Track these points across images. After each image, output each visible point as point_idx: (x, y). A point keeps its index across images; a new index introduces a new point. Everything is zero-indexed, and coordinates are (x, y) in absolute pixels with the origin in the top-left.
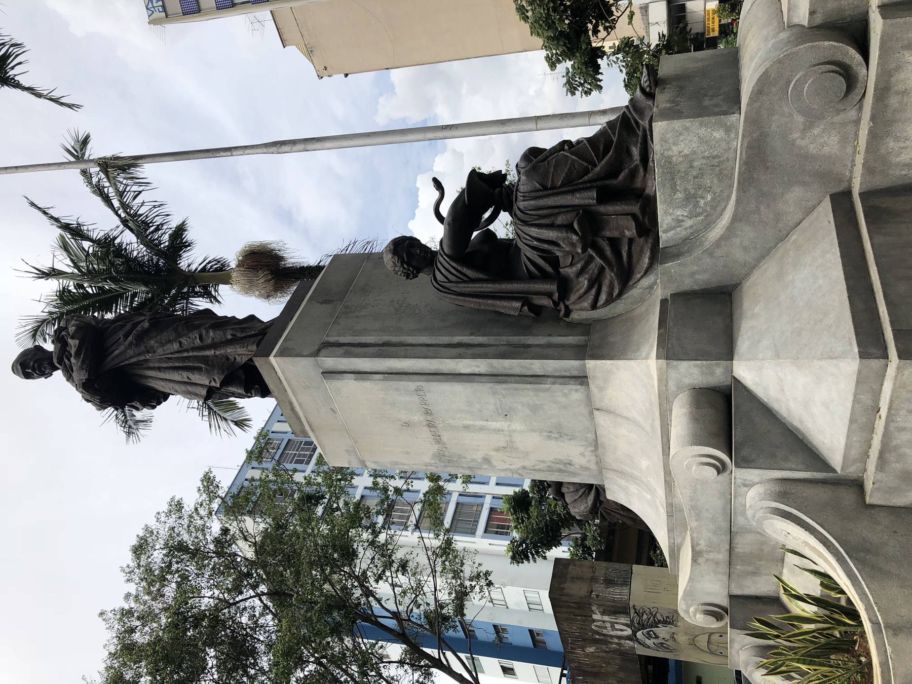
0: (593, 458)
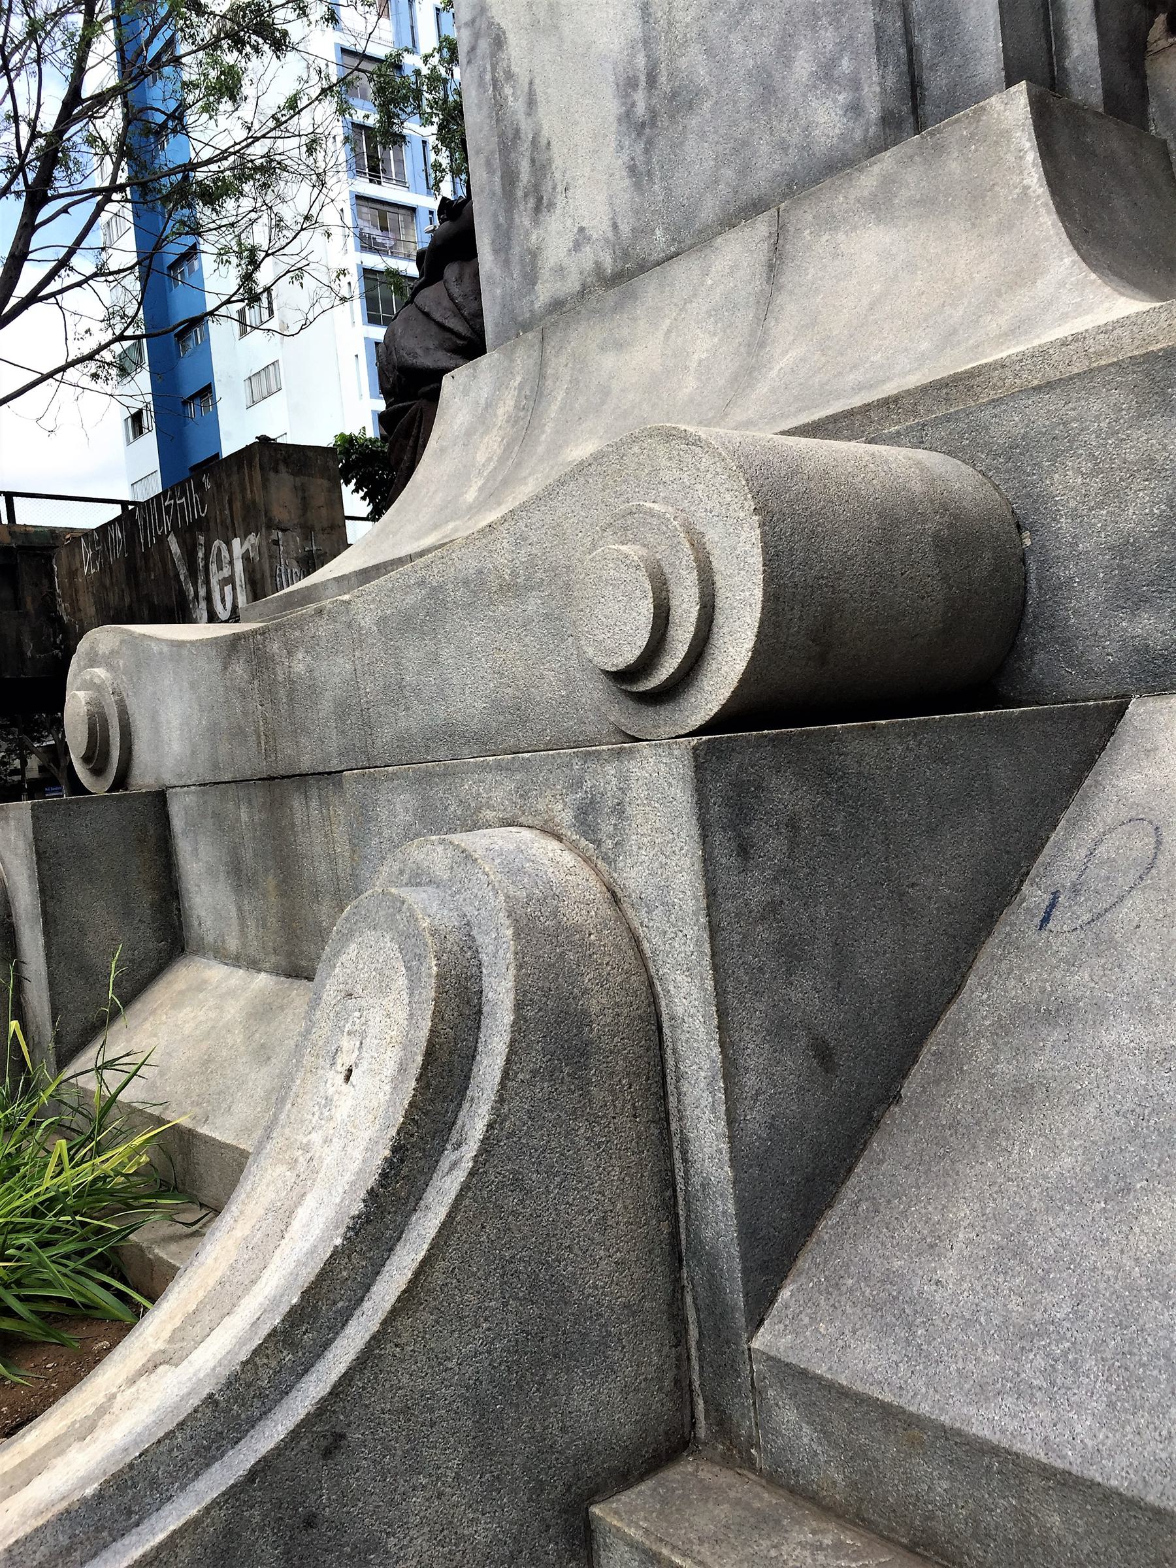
0: (572, 284)
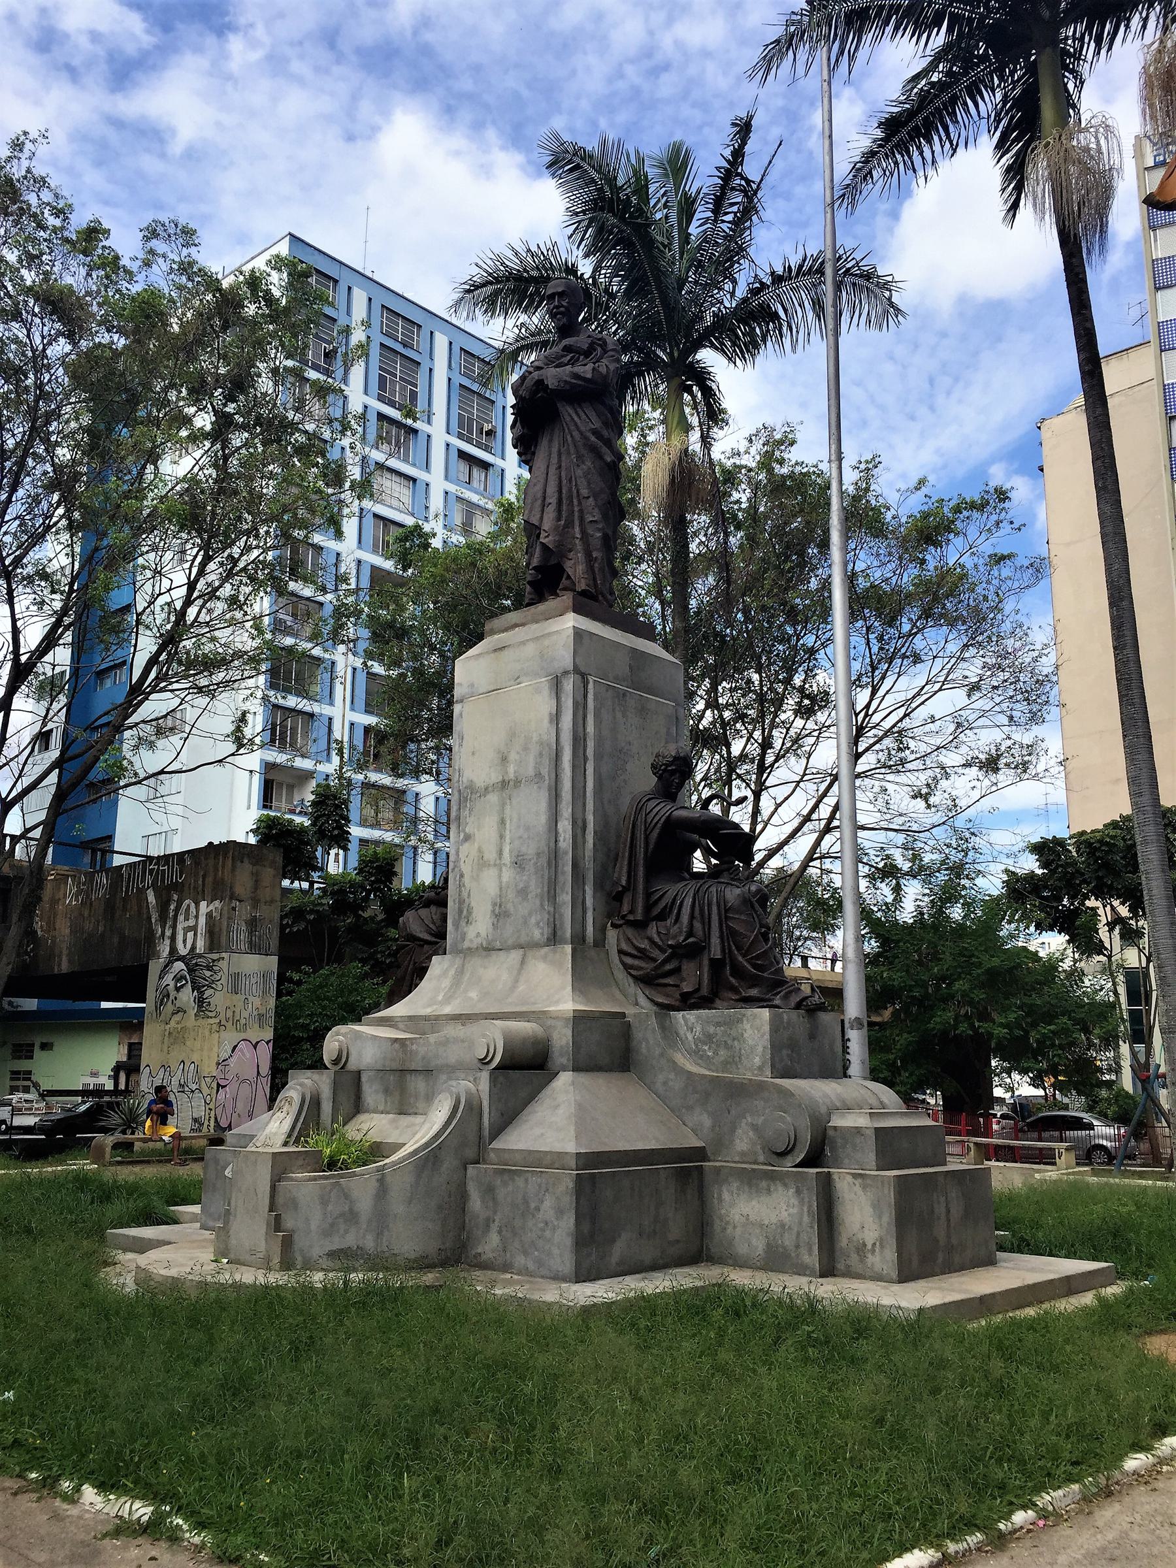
0: (474, 946)
